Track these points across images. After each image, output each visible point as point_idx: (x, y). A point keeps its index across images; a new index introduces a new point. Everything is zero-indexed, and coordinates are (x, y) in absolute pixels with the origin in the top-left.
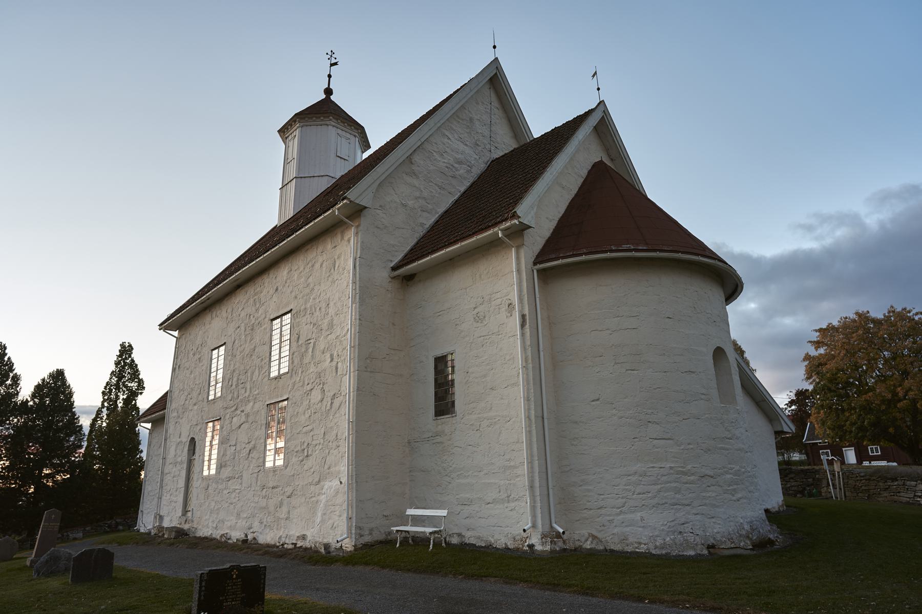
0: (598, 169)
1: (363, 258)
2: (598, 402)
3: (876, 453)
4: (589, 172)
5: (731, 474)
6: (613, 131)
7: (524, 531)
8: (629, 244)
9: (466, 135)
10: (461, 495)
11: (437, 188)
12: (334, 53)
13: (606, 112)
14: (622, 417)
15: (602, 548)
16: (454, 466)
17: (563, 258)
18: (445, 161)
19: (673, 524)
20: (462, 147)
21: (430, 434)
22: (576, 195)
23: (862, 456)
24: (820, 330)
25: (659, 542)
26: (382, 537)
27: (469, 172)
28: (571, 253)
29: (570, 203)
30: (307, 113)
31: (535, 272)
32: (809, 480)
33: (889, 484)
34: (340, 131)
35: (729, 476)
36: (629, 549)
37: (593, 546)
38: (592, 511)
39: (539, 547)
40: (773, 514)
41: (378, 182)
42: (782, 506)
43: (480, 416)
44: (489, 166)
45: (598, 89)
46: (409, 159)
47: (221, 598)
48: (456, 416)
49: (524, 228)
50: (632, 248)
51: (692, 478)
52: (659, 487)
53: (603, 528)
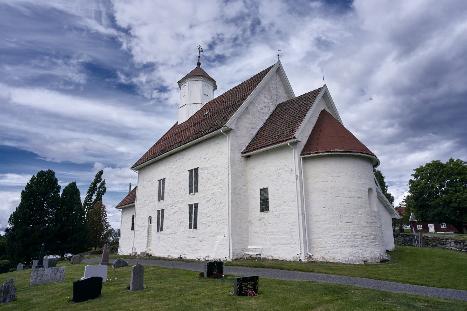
0: (323, 112)
1: (231, 149)
2: (325, 208)
3: (444, 227)
4: (320, 115)
5: (373, 235)
6: (329, 97)
7: (298, 254)
8: (337, 149)
9: (267, 95)
10: (271, 242)
11: (257, 118)
12: (201, 46)
13: (327, 89)
14: (333, 214)
15: (326, 261)
16: (269, 231)
17: (312, 154)
18: (260, 107)
19: (351, 253)
20: (266, 100)
21: (259, 219)
22: (315, 125)
23: (437, 229)
24: (416, 170)
25: (347, 259)
26: (241, 257)
27: (269, 110)
28: (315, 152)
29: (313, 129)
30: (191, 75)
31: (301, 158)
32: (407, 239)
33: (440, 241)
34: (205, 83)
35: (372, 236)
36: (336, 262)
37: (323, 260)
38: (322, 248)
39: (303, 260)
40: (391, 252)
41: (237, 119)
42: (394, 249)
43: (279, 212)
44: (276, 107)
45: (324, 80)
46: (247, 108)
47: (212, 271)
48: (269, 212)
49: (297, 142)
50: (339, 151)
51: (359, 237)
52: (347, 240)
53: (326, 254)
